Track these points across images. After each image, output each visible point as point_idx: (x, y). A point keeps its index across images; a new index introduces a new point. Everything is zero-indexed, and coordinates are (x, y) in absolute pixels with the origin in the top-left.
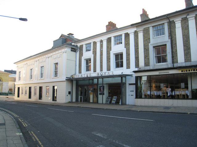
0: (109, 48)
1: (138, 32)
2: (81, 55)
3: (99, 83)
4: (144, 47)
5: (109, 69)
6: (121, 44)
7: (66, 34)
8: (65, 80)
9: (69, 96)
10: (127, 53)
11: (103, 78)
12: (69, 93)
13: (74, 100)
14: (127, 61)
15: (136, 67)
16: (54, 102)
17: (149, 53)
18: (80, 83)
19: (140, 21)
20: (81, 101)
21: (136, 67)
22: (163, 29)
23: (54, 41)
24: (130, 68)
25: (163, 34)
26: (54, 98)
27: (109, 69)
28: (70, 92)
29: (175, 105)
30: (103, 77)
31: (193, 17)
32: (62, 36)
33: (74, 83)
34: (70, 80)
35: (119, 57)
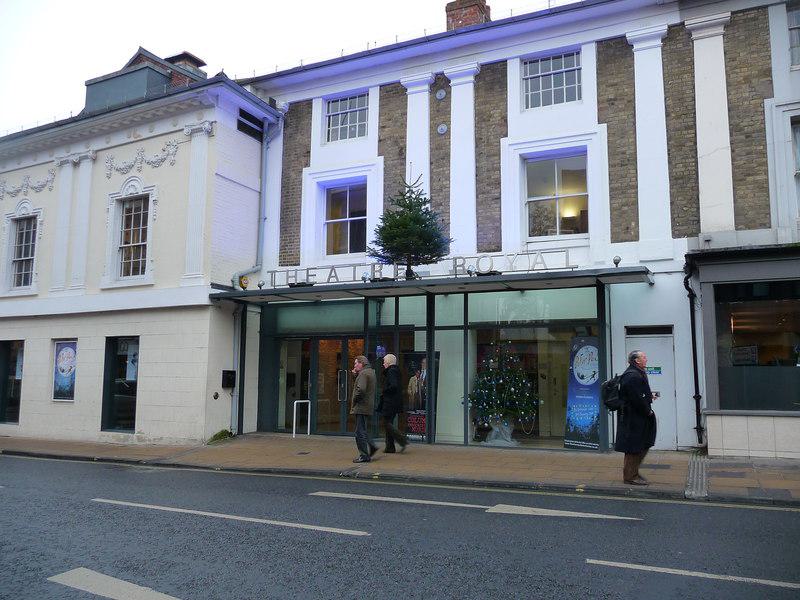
0: (491, 126)
1: (694, 35)
2: (297, 157)
3: (437, 324)
4: (730, 117)
5: (490, 242)
6: (566, 106)
7: (164, 49)
8: (205, 301)
9: (227, 401)
10: (613, 152)
11: (466, 294)
12: (229, 380)
13: (251, 423)
14: (611, 198)
15: (676, 234)
16: (114, 437)
17: (764, 154)
18: (293, 320)
19: (442, 28)
20: (302, 422)
21: (676, 234)
22: (364, 112)
23: (91, 85)
24: (636, 238)
25: (363, 132)
26: (120, 407)
27: (490, 242)
28: (233, 373)
29: (280, 414)
30: (492, 282)
31: (467, 74)
32: (141, 56)
33: (254, 319)
34: (231, 303)
35: (556, 169)
